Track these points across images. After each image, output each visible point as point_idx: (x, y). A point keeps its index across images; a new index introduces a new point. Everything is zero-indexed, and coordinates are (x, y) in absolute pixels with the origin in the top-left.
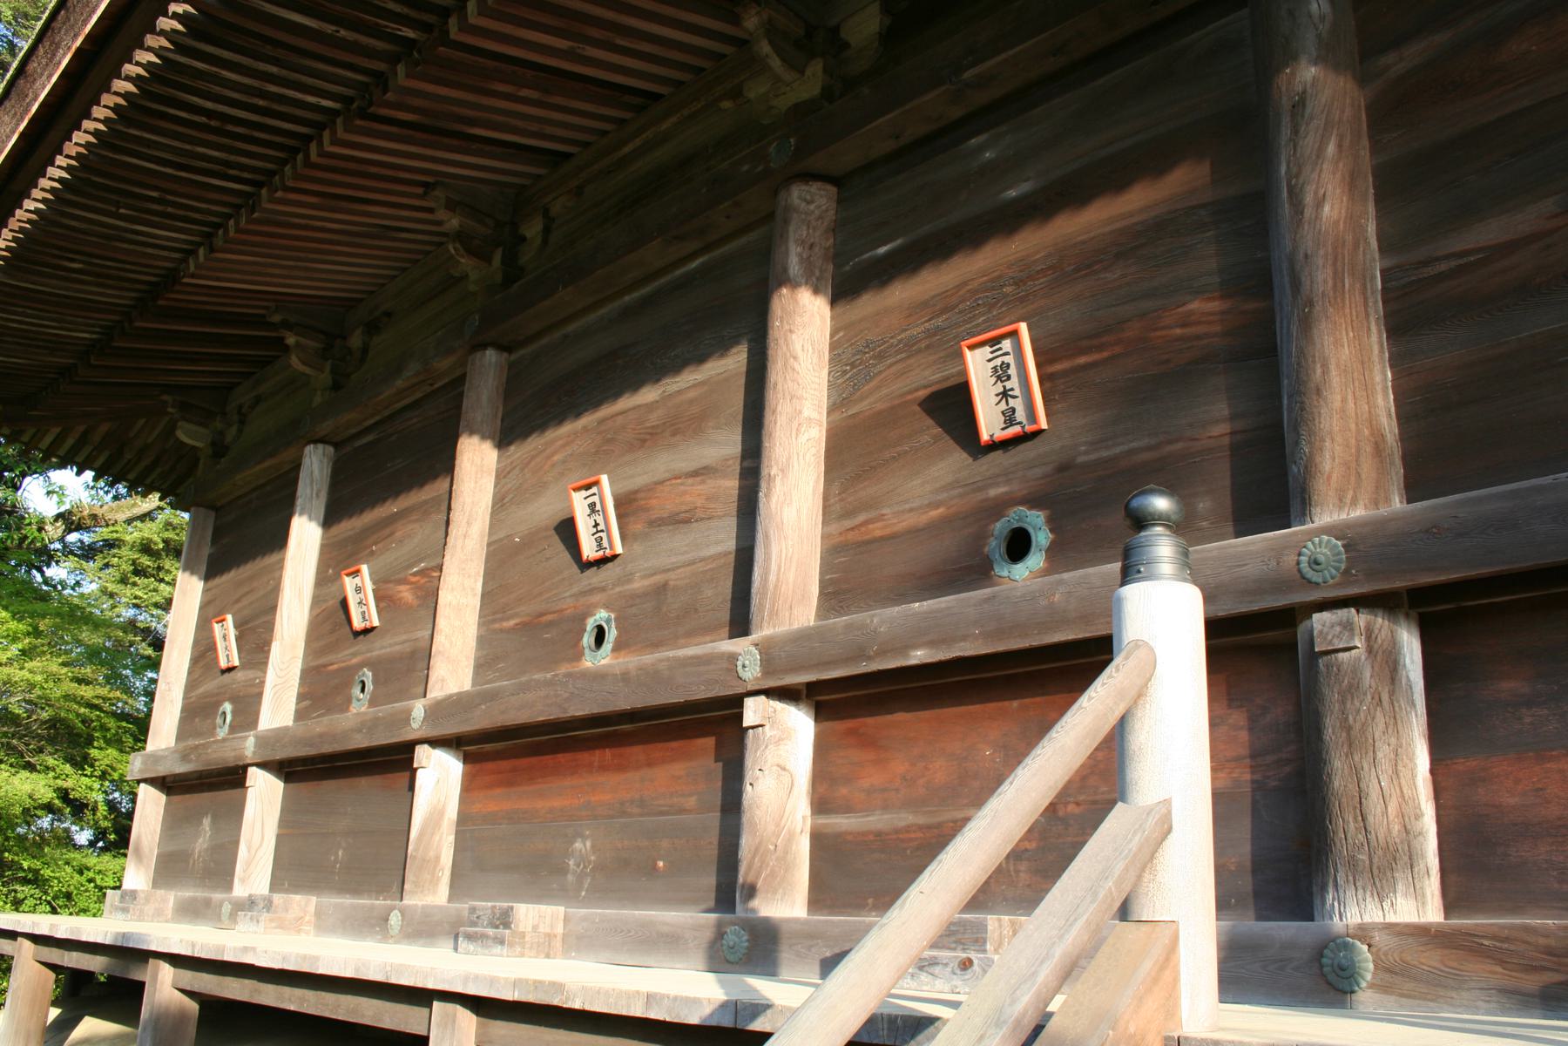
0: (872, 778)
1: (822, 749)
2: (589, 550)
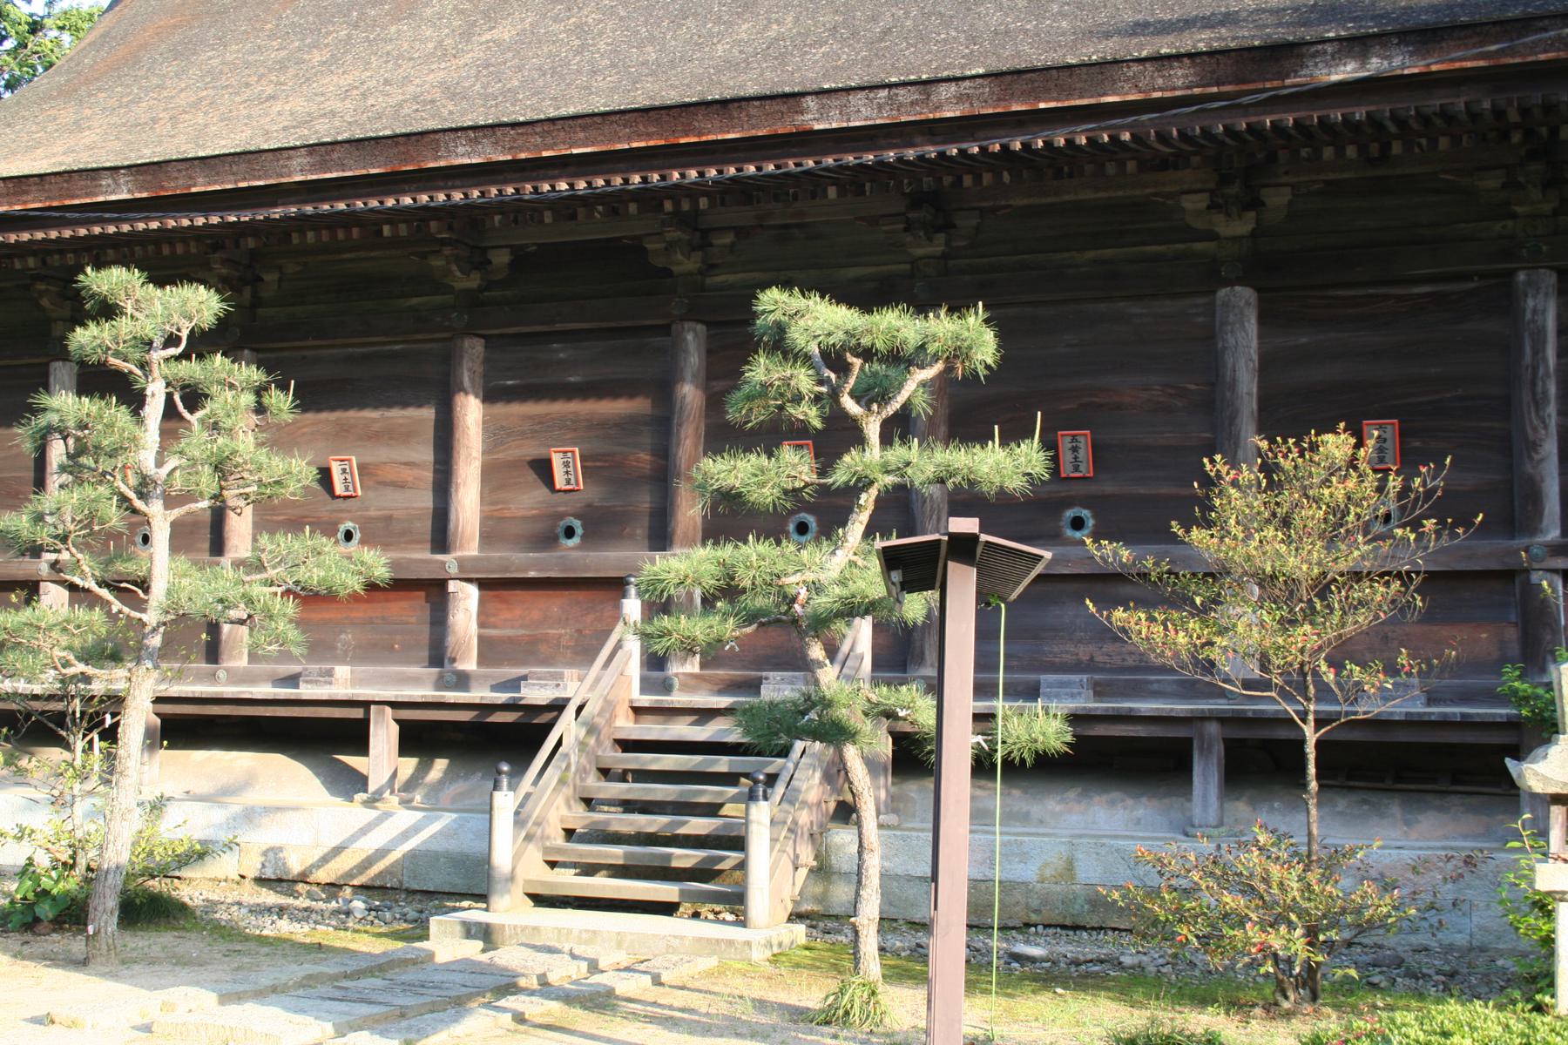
0: (506, 615)
1: (482, 602)
2: (339, 489)
